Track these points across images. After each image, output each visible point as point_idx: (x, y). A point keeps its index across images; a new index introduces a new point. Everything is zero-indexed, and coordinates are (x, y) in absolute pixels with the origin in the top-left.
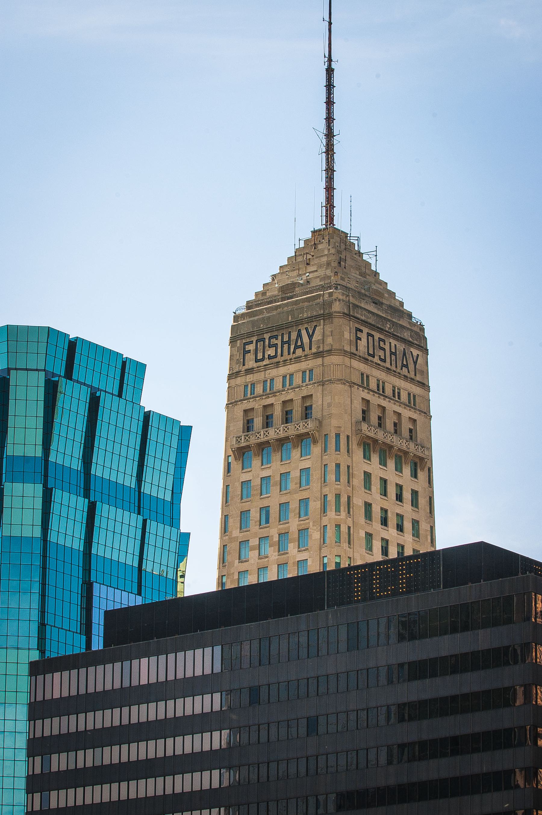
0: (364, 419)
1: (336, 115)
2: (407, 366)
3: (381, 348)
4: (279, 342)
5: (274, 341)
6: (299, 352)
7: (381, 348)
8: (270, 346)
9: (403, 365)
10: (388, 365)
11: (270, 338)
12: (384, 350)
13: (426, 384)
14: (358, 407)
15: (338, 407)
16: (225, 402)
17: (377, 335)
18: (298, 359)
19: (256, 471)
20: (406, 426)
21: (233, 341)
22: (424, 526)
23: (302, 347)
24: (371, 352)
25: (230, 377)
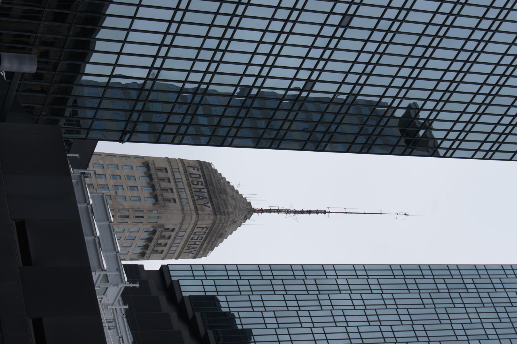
0: (165, 229)
1: (264, 214)
2: (189, 249)
3: (198, 238)
4: (200, 186)
5: (200, 183)
6: (196, 198)
7: (198, 238)
8: (198, 182)
9: (189, 247)
10: (190, 240)
11: (193, 184)
12: (197, 239)
13: (181, 257)
14: (171, 227)
15: (172, 218)
16: (170, 157)
17: (204, 236)
18: (193, 197)
19: (140, 172)
20: (160, 249)
21: (199, 162)
22: (80, 203)
23: (199, 199)
24: (197, 233)
25: (182, 160)
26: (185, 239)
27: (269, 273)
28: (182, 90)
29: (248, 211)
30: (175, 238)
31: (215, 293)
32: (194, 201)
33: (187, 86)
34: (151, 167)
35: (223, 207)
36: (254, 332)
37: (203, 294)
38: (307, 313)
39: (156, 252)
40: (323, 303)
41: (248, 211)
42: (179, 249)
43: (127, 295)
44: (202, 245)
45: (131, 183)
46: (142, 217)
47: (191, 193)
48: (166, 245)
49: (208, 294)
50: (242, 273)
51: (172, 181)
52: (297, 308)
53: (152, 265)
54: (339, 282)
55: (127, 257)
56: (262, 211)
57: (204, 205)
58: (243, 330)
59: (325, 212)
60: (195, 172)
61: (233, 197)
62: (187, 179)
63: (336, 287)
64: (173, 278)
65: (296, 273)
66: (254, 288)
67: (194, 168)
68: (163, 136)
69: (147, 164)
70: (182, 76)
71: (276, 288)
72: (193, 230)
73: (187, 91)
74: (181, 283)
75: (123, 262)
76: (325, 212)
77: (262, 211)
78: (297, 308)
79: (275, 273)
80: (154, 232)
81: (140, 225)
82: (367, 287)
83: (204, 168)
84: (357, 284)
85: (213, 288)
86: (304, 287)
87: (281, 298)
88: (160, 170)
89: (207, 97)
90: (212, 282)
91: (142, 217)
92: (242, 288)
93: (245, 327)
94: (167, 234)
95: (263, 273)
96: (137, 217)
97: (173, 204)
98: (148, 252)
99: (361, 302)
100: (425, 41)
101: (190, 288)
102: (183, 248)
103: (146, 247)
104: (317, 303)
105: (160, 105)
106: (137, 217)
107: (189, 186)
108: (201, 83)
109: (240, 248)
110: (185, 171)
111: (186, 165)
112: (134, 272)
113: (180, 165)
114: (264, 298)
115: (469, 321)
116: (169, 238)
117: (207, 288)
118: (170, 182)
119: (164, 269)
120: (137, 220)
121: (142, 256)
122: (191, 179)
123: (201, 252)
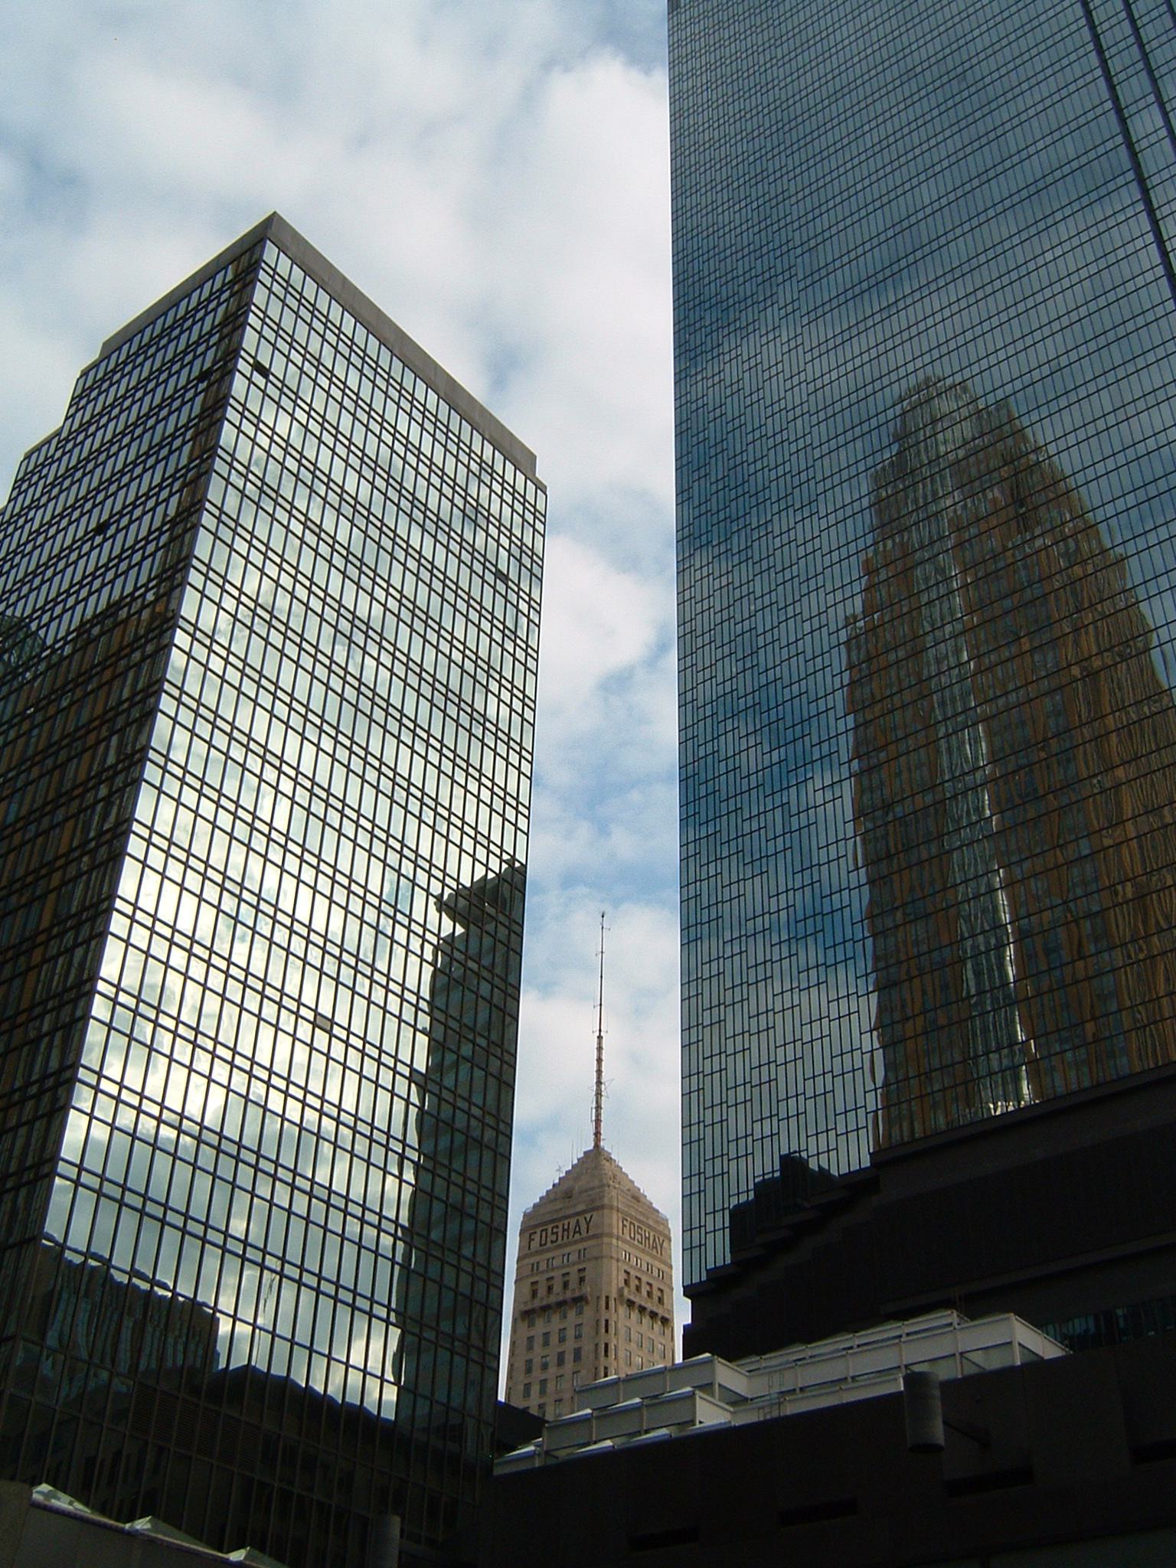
18: (576, 1242)
19: (540, 1327)
20: (656, 1294)
26: (640, 1255)
27: (695, 1128)
28: (405, 1266)
29: (595, 1160)
30: (640, 1270)
31: (727, 1212)
32: (582, 1240)
33: (399, 1258)
34: (529, 1307)
35: (589, 1193)
36: (785, 1151)
37: (727, 1231)
38: (756, 1072)
39: (660, 1300)
40: (739, 1048)
41: (595, 1160)
42: (657, 1264)
43: (732, 1353)
44: (649, 1227)
45: (554, 1339)
46: (606, 1345)
47: (570, 1244)
48: (650, 1285)
49: (727, 1224)
50: (695, 1171)
51: (551, 1274)
52: (748, 1086)
53: (682, 1313)
54: (707, 1022)
55: (669, 1345)
56: (597, 1134)
57: (588, 1224)
58: (782, 1170)
59: (600, 1037)
60: (537, 1237)
61: (577, 1179)
62: (549, 1250)
63: (716, 1076)
64: (704, 1278)
65: (694, 1087)
66: (718, 1153)
67: (531, 1240)
68: (504, 1078)
69: (525, 1315)
70: (384, 1266)
71: (717, 1119)
72: (624, 1241)
73: (407, 1256)
74: (710, 1266)
75: (679, 1359)
76: (600, 1037)
77: (597, 1134)
78: (748, 1086)
79: (694, 1120)
80: (631, 1304)
81: (619, 1325)
82: (715, 980)
83: (532, 1226)
84: (711, 1041)
85: (719, 1215)
86: (716, 1076)
87: (731, 1059)
88: (534, 1294)
89: (409, 1313)
90: (710, 1218)
91: (606, 1345)
92: (718, 1171)
93: (777, 1166)
94: (634, 1283)
95: (695, 1137)
96: (606, 1355)
97: (586, 1273)
98: (660, 1311)
99: (737, 990)
100: (357, 765)
101: (719, 1252)
102: (654, 1257)
103: (653, 1315)
104: (739, 1056)
105: (428, 1301)
106: (607, 1307)
107: (560, 1247)
108: (395, 1236)
109: (658, 1176)
110: (537, 1253)
111: (526, 1251)
112: (693, 1341)
113: (527, 1261)
114: (732, 1137)
115: (763, 831)
116: (640, 1279)
117: (719, 1225)
118: (552, 1278)
119: (688, 1291)
120: (612, 1330)
121: (666, 1322)
122: (549, 1244)
123: (661, 1228)
